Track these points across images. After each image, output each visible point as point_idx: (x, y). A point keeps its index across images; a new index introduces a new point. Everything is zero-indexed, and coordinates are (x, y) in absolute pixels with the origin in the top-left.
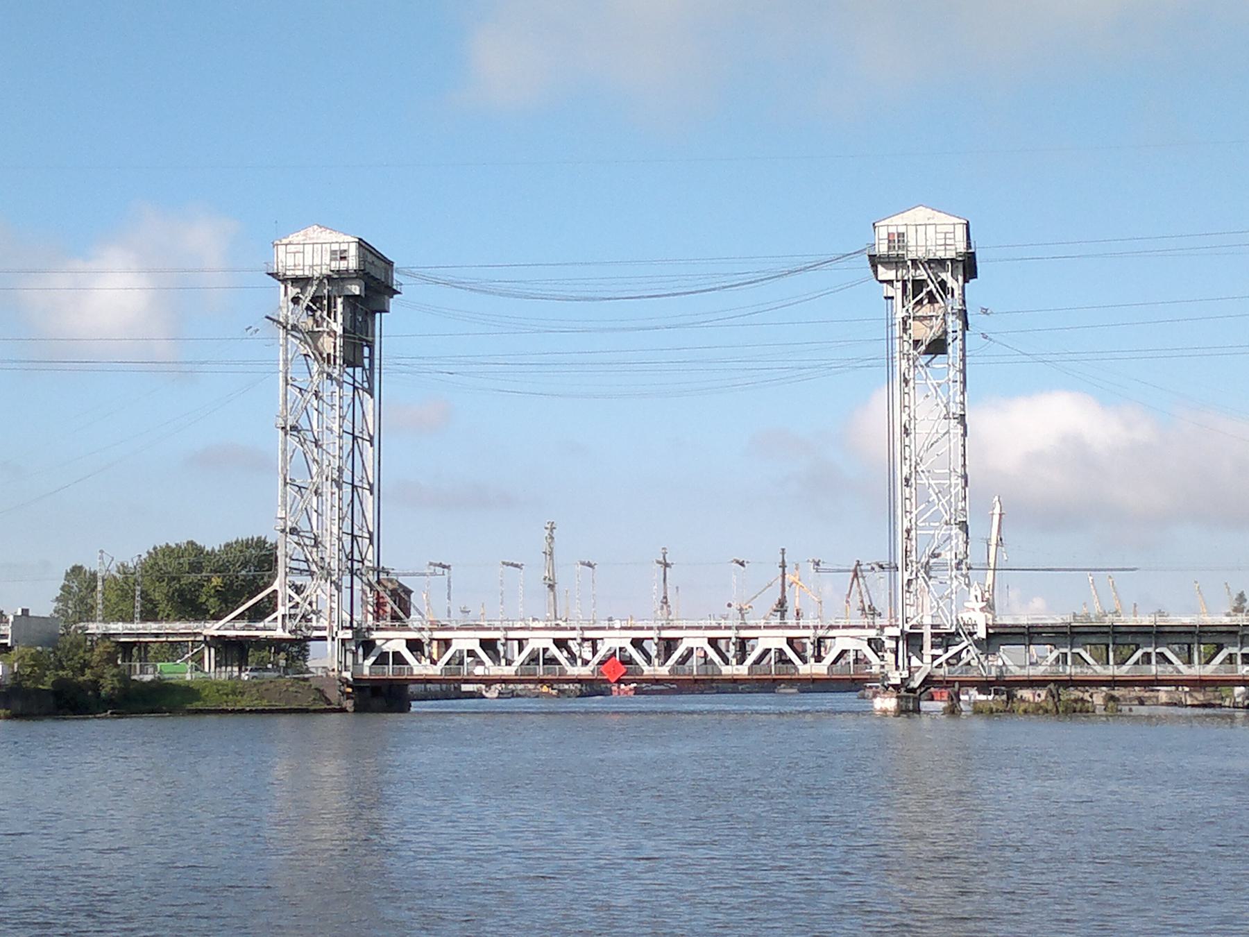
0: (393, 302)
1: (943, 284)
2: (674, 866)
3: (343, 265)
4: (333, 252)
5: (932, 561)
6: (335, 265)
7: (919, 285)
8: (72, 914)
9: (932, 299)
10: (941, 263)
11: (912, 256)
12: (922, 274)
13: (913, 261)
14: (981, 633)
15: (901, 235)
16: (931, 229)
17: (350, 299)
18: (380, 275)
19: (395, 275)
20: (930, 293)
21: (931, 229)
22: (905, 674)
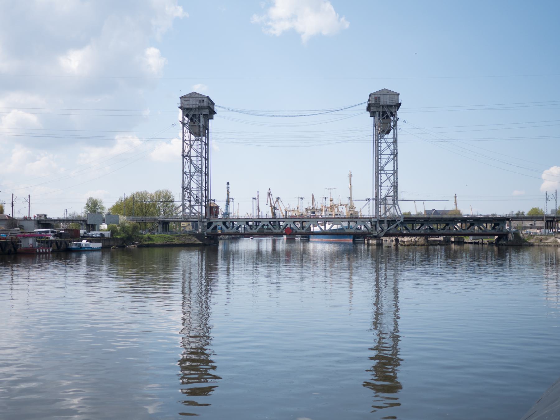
0: (215, 116)
3: (202, 104)
4: (200, 101)
7: (384, 113)
10: (391, 106)
13: (383, 106)
14: (402, 220)
15: (379, 98)
19: (215, 107)
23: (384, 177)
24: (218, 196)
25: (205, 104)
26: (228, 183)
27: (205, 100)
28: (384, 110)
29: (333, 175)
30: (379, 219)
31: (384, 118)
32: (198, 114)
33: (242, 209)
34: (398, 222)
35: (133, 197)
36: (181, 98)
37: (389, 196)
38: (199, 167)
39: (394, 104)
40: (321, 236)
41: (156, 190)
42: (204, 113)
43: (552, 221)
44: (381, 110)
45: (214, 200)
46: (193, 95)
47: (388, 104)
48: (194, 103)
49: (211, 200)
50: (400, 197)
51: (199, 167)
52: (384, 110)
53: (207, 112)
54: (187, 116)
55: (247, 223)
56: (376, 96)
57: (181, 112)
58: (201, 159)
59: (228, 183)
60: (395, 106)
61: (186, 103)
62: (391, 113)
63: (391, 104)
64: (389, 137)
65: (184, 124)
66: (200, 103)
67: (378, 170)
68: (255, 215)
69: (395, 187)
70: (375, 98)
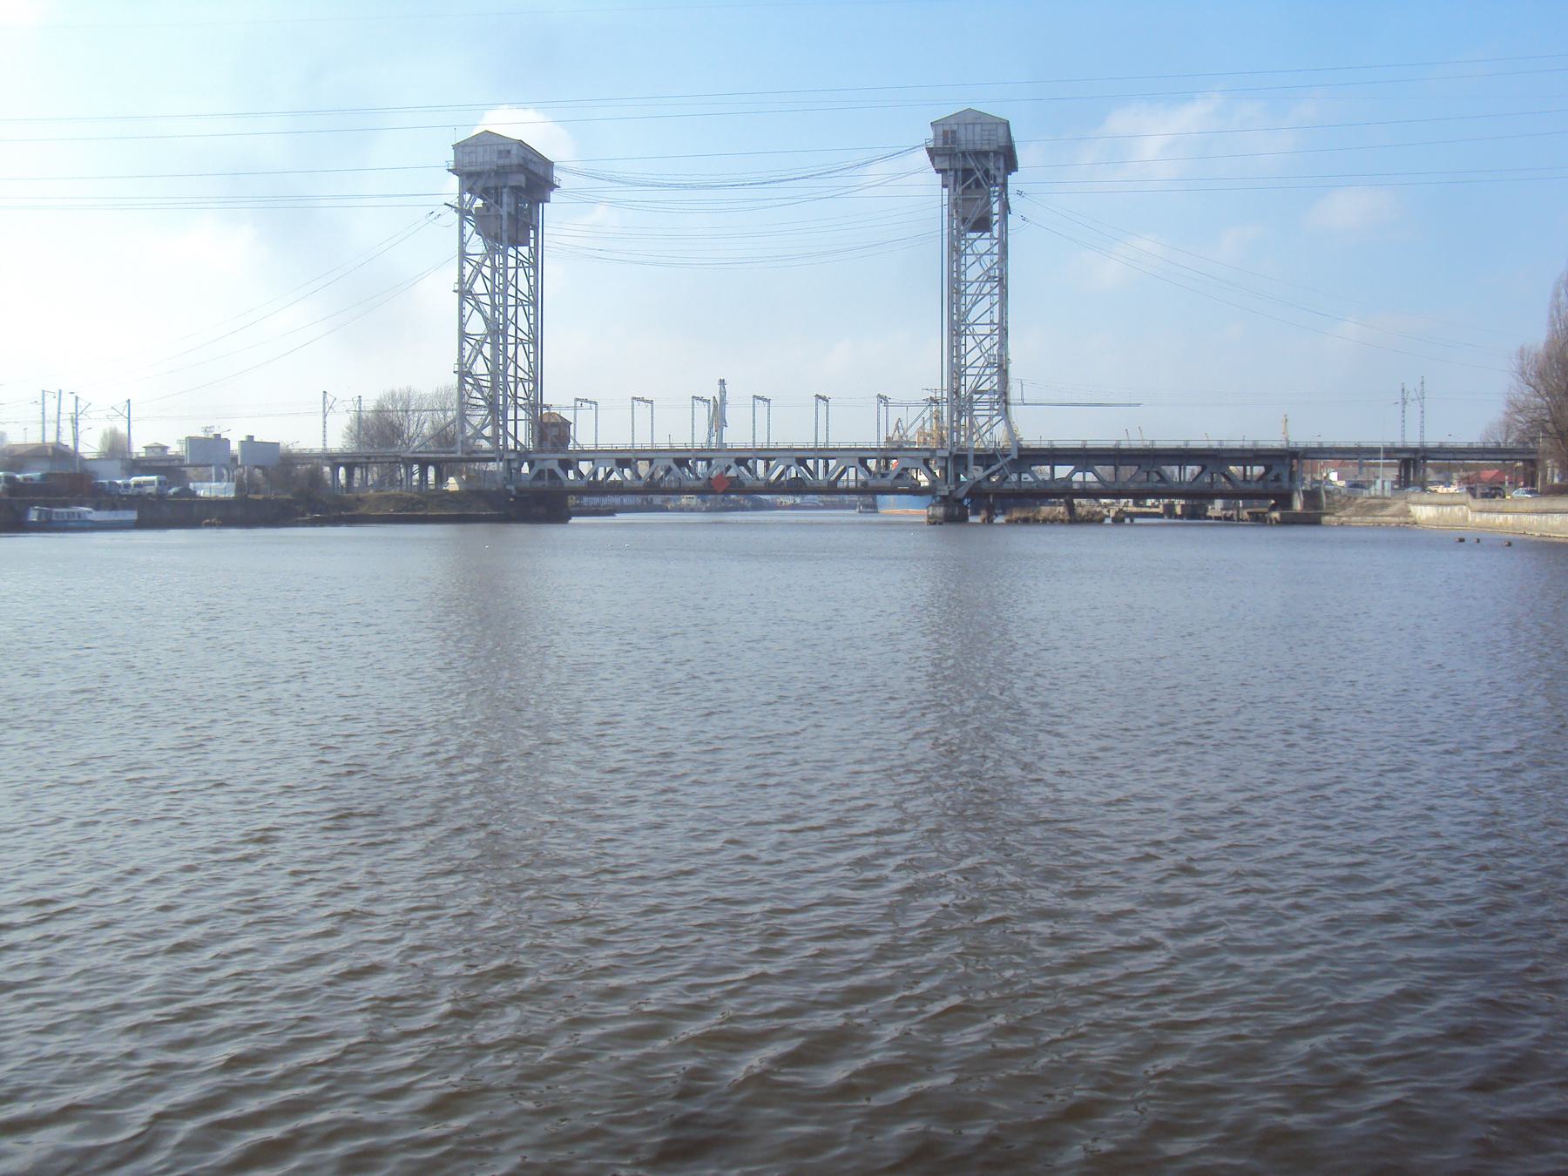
0: (553, 195)
1: (987, 172)
2: (1364, 881)
3: (506, 161)
4: (500, 152)
5: (976, 397)
6: (501, 162)
7: (968, 173)
8: (214, 721)
9: (978, 184)
10: (986, 154)
11: (963, 148)
12: (972, 164)
13: (964, 154)
14: (1015, 455)
15: (954, 132)
16: (978, 128)
17: (516, 190)
18: (540, 171)
19: (555, 173)
20: (977, 181)
21: (978, 128)
22: (953, 487)
25: (515, 160)
26: (722, 382)
27: (514, 150)
28: (975, 167)
30: (955, 451)
31: (969, 187)
34: (1002, 462)
35: (380, 411)
36: (455, 147)
37: (983, 392)
38: (503, 330)
39: (994, 147)
41: (388, 390)
44: (959, 165)
45: (548, 407)
46: (487, 139)
47: (978, 147)
48: (487, 158)
49: (543, 406)
50: (1014, 394)
51: (503, 330)
52: (975, 167)
54: (470, 191)
55: (863, 462)
56: (947, 128)
57: (455, 180)
58: (505, 300)
59: (722, 382)
60: (996, 153)
61: (466, 160)
63: (986, 148)
65: (463, 213)
66: (499, 157)
67: (957, 329)
70: (945, 133)
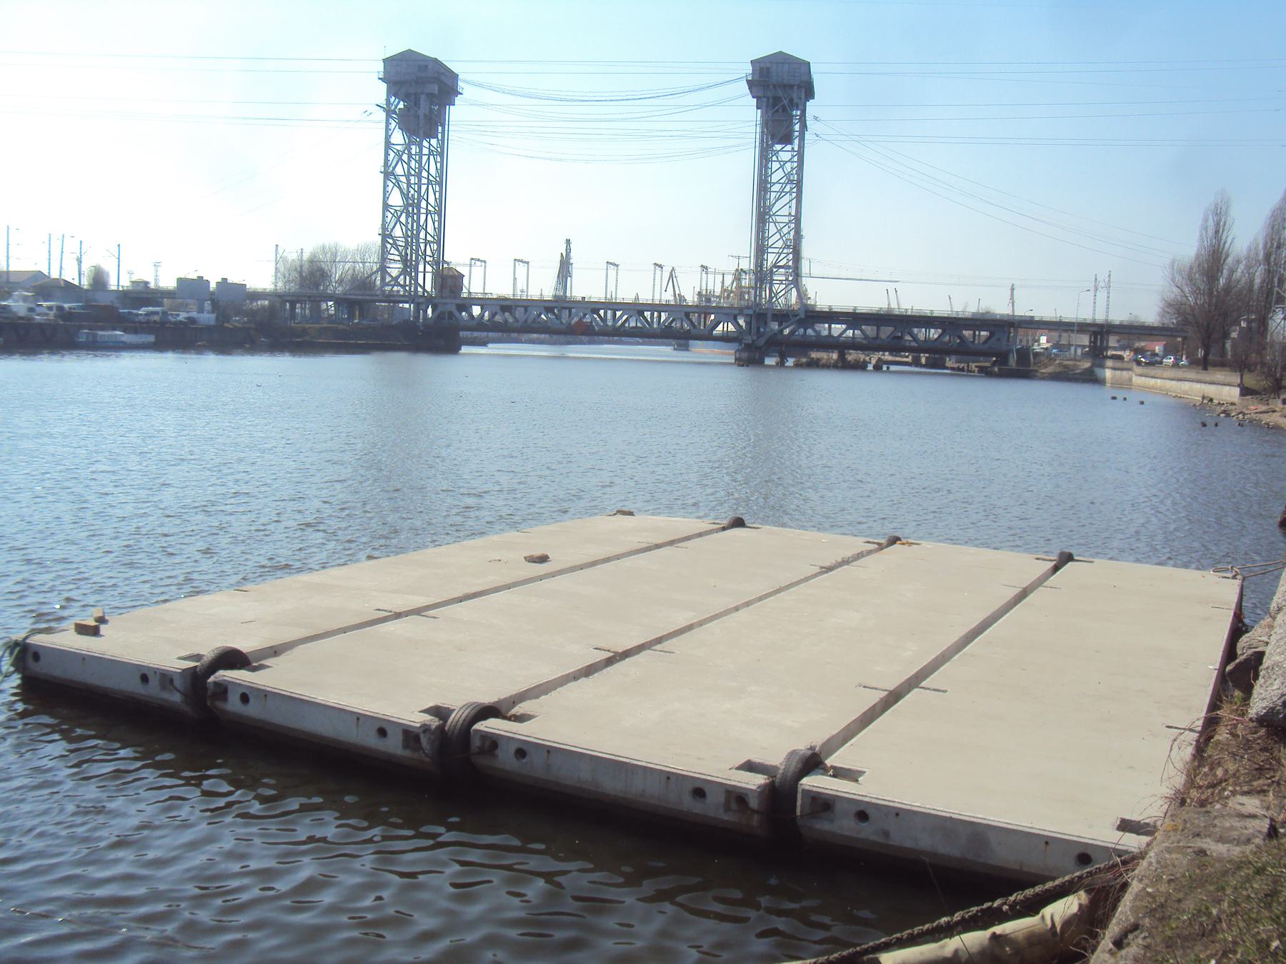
0: (458, 100)
10: (791, 87)
14: (803, 316)
19: (460, 83)
23: (772, 229)
24: (455, 255)
29: (673, 224)
32: (421, 93)
33: (489, 280)
40: (718, 343)
42: (428, 91)
43: (1101, 333)
50: (805, 268)
52: (781, 93)
53: (435, 89)
60: (799, 87)
62: (791, 100)
64: (785, 153)
67: (763, 216)
68: (668, 297)
69: (796, 250)
